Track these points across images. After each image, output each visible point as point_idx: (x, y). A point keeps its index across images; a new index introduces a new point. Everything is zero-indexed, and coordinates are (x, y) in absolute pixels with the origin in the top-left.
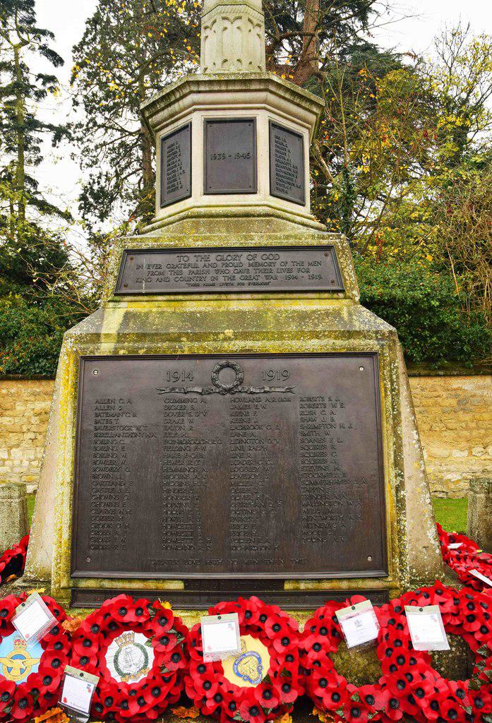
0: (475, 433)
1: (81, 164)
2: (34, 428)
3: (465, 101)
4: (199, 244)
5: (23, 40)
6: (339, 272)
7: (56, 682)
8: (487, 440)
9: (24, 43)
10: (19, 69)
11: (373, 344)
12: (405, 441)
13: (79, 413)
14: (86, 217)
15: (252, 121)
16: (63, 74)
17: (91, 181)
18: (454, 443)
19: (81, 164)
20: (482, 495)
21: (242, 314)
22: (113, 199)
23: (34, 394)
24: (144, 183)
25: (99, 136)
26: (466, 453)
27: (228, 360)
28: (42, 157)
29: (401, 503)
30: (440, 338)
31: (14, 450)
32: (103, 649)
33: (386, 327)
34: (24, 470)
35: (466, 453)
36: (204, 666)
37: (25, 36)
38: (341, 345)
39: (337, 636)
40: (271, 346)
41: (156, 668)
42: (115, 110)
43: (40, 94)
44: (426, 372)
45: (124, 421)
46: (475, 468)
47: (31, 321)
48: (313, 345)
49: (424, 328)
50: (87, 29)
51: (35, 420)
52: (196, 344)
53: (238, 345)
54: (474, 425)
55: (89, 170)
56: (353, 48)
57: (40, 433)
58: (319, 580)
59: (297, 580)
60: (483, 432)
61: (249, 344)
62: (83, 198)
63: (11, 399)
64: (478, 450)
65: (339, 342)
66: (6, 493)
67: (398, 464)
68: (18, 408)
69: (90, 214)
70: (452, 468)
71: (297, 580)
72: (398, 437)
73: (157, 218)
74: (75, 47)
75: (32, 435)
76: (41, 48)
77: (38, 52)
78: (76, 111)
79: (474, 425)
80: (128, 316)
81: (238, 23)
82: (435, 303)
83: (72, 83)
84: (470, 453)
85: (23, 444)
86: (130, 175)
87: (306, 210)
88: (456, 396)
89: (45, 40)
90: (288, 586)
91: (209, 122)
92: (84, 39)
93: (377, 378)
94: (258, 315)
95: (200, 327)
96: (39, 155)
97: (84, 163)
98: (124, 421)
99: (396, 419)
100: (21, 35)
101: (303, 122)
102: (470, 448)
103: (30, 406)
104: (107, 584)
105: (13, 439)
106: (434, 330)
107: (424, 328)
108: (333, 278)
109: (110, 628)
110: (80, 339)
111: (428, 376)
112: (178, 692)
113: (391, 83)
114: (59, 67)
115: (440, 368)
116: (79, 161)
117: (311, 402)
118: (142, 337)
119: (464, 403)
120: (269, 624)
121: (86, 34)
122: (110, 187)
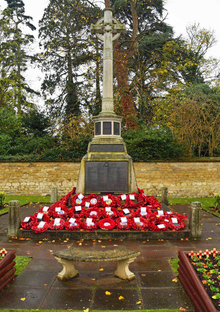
0: (178, 179)
1: (42, 69)
2: (46, 176)
3: (197, 53)
4: (102, 143)
5: (19, 20)
6: (124, 148)
7: (84, 204)
8: (181, 181)
9: (20, 21)
10: (17, 31)
11: (128, 160)
12: (132, 174)
13: (85, 169)
14: (44, 92)
15: (111, 122)
16: (35, 33)
17: (46, 77)
18: (171, 182)
19: (42, 69)
20: (164, 191)
21: (109, 155)
22: (56, 85)
23: (47, 166)
24: (69, 79)
25: (49, 58)
26: (175, 185)
27: (107, 162)
28: (27, 68)
29: (131, 182)
30: (167, 151)
31: (41, 183)
32: (90, 200)
33: (130, 157)
34: (44, 189)
35: (175, 185)
36: (104, 202)
37: (20, 18)
38: (123, 160)
39: (121, 199)
40: (113, 160)
41: (97, 202)
42: (56, 47)
43: (27, 42)
44: (163, 161)
45: (92, 170)
46: (177, 190)
47: (41, 143)
48: (119, 160)
49: (162, 148)
50: (45, 13)
51: (47, 174)
52: (102, 159)
53: (108, 160)
54: (177, 177)
55: (45, 73)
56: (157, 23)
57: (49, 178)
58: (119, 192)
59: (116, 192)
60: (180, 179)
61: (110, 159)
62: (43, 84)
63: (40, 168)
64: (179, 184)
65: (123, 159)
66: (54, 189)
67: (131, 177)
68: (42, 170)
69: (45, 90)
70: (171, 189)
71: (116, 192)
72: (131, 173)
73: (95, 137)
74: (40, 21)
75: (46, 179)
76: (26, 23)
77: (25, 25)
78: (41, 49)
79: (177, 177)
80: (92, 155)
81: (109, 102)
82: (165, 141)
83: (39, 38)
84: (176, 185)
85: (44, 181)
86: (62, 75)
87: (120, 136)
88: (172, 168)
89: (28, 20)
90: (115, 193)
91: (104, 122)
92: (43, 17)
93: (128, 165)
94: (111, 155)
95: (103, 156)
96: (25, 67)
97: (43, 69)
98: (92, 170)
99: (131, 170)
100: (18, 17)
101: (119, 121)
102: (176, 184)
103: (46, 170)
104: (90, 193)
105: (40, 180)
106: (165, 149)
107: (162, 148)
108: (123, 149)
109: (92, 198)
110: (85, 159)
111: (164, 162)
112: (100, 205)
113: (167, 46)
114: (34, 31)
115: (167, 160)
116: (41, 68)
117: (118, 168)
118: (94, 158)
119: (174, 170)
120: (112, 197)
121: (44, 15)
122: (54, 80)
